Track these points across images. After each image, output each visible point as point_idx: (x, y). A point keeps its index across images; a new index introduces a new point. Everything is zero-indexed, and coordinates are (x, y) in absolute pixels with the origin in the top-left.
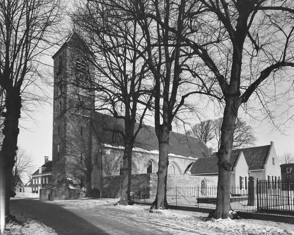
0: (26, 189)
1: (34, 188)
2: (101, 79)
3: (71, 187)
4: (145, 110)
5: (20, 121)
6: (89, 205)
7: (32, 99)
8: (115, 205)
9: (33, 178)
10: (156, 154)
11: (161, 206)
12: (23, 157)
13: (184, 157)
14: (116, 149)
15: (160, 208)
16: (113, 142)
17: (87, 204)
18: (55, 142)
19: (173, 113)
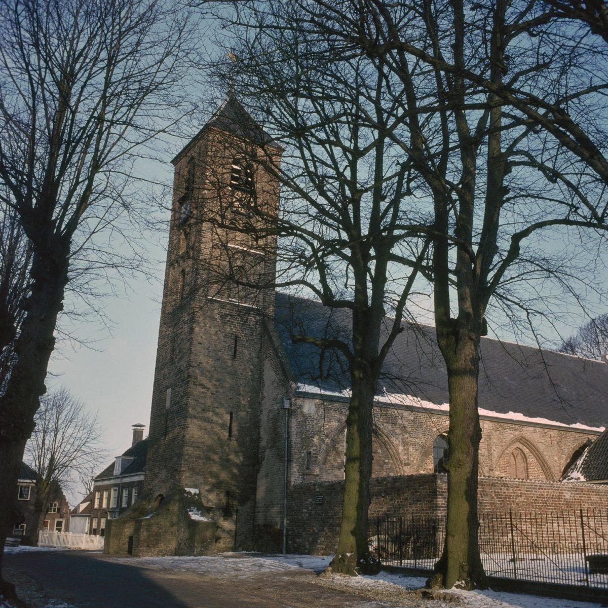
0: (76, 522)
1: (95, 521)
2: (293, 208)
3: (195, 516)
4: (411, 279)
5: (62, 320)
6: (240, 571)
7: (103, 265)
8: (319, 572)
9: (97, 489)
10: (443, 413)
11: (460, 577)
12: (73, 424)
13: (558, 424)
14: (332, 399)
15: (457, 583)
16: (320, 376)
17: (236, 570)
18: (161, 382)
19: (489, 285)
